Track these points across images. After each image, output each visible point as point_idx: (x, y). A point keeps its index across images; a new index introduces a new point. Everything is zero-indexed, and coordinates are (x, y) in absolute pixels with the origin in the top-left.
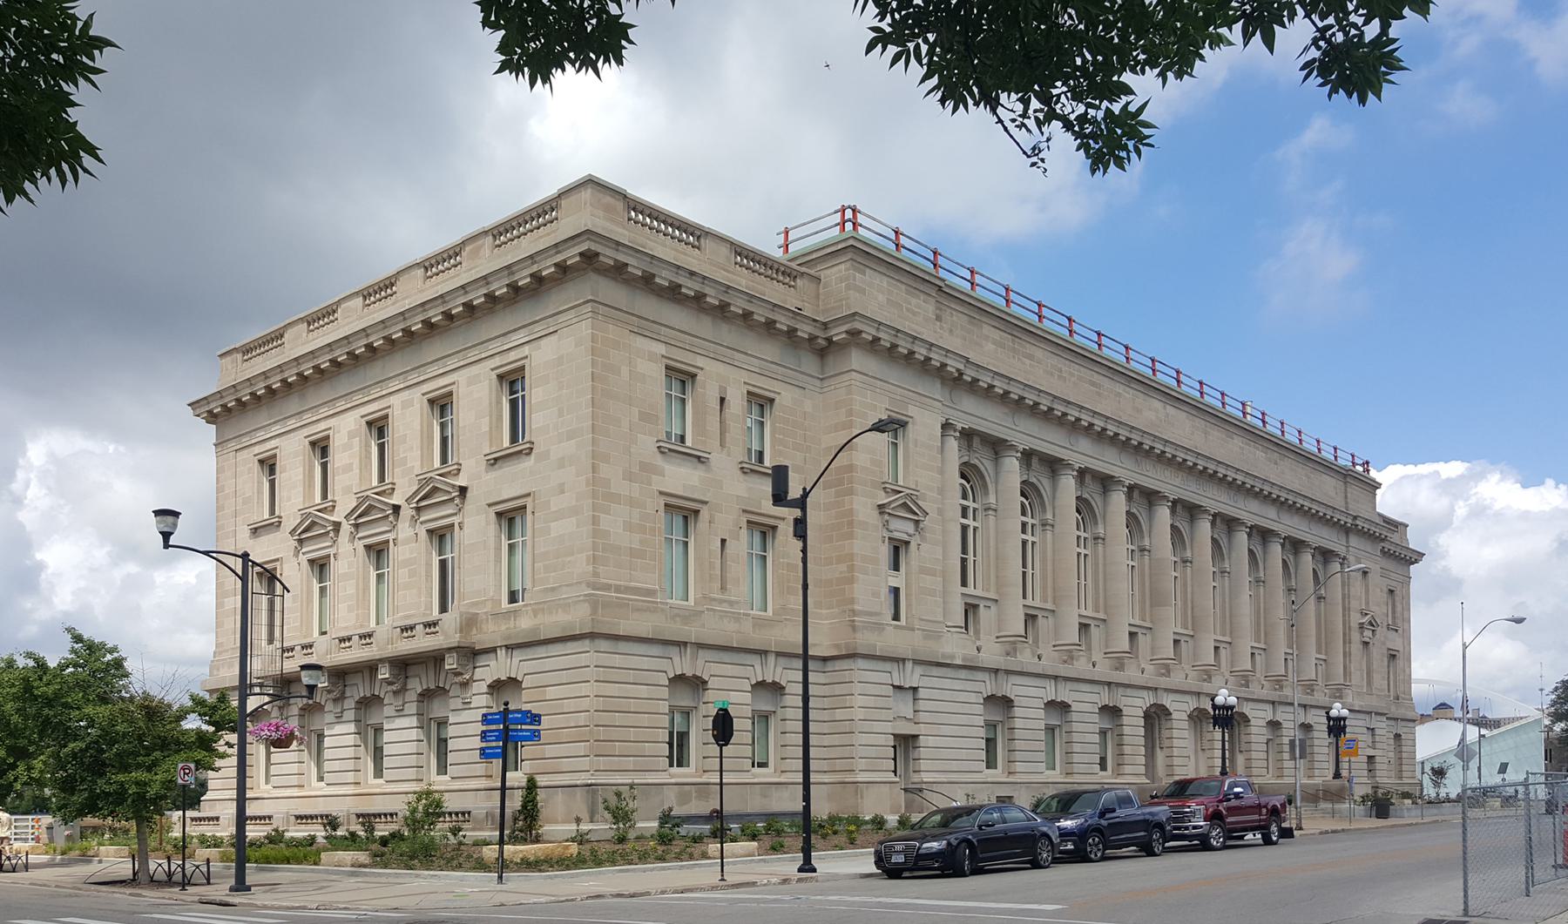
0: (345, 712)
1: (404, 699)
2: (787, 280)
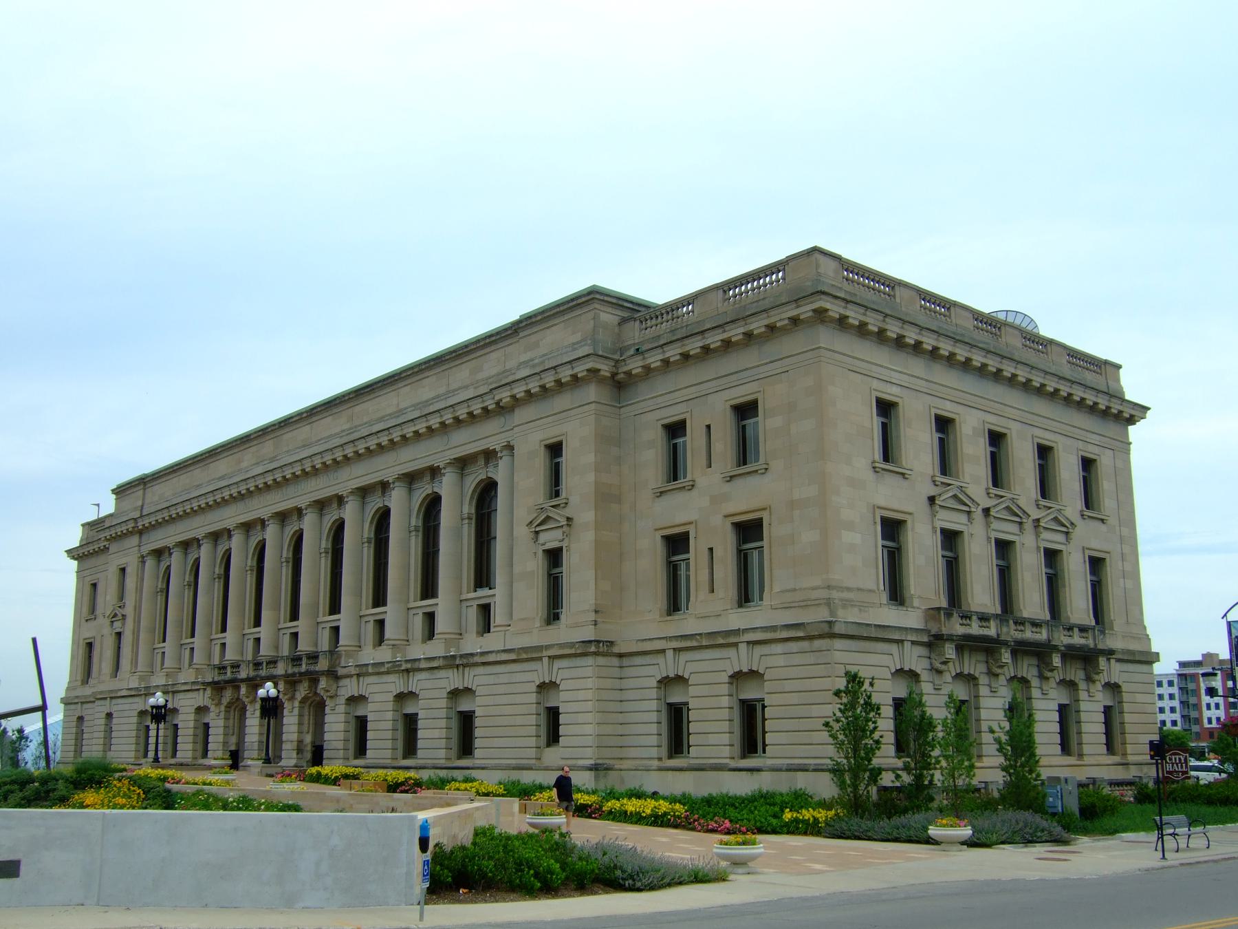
0: (337, 707)
1: (254, 707)
2: (654, 322)
